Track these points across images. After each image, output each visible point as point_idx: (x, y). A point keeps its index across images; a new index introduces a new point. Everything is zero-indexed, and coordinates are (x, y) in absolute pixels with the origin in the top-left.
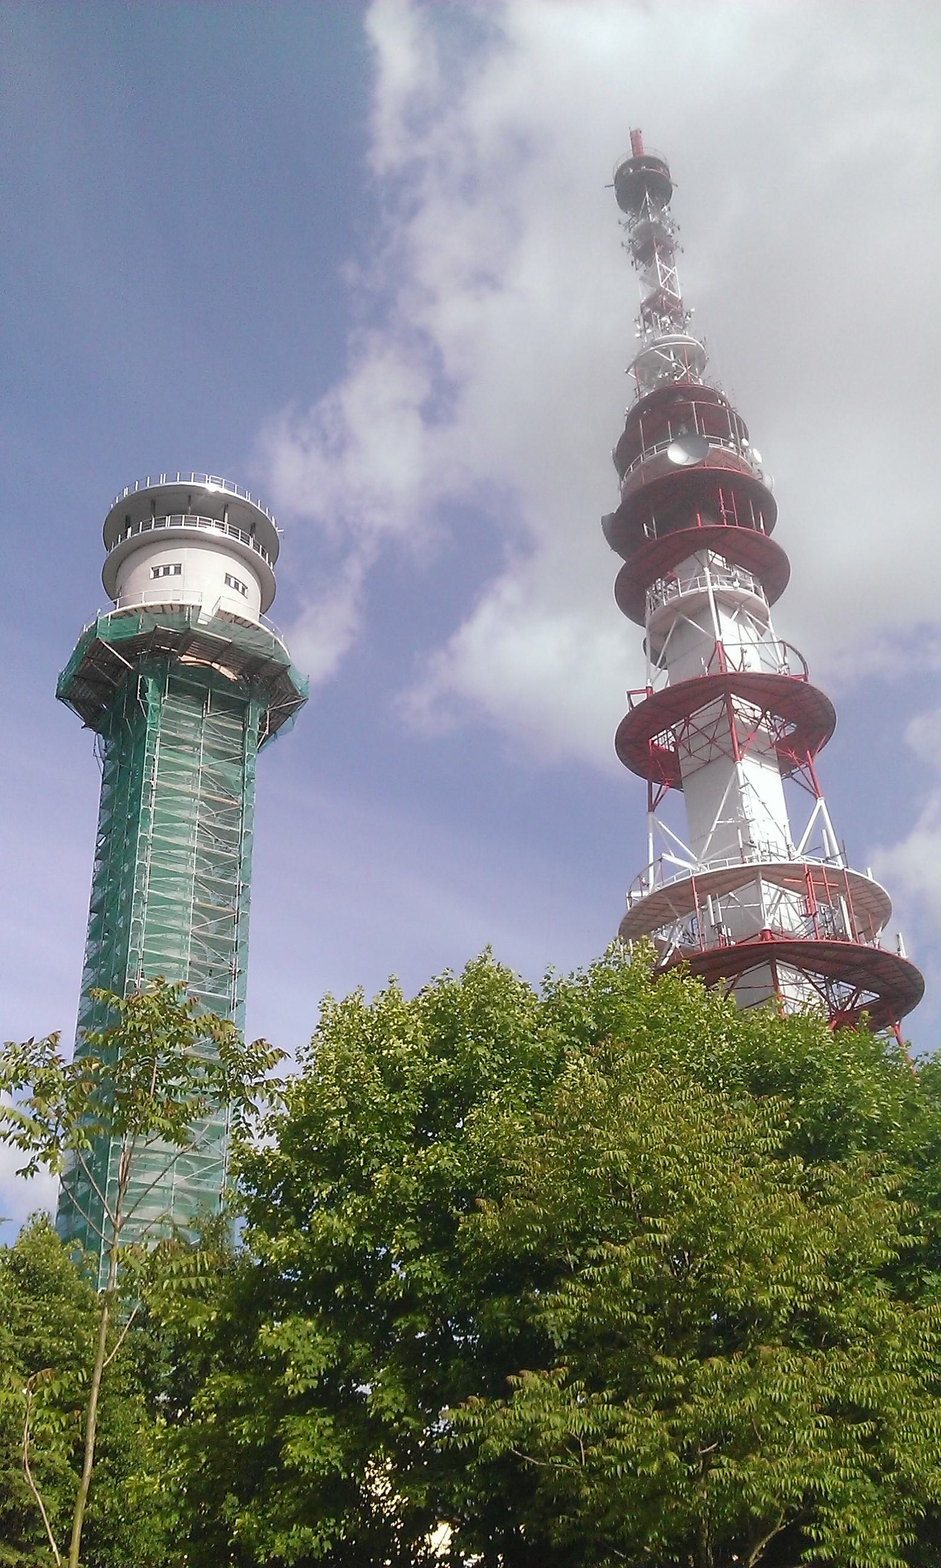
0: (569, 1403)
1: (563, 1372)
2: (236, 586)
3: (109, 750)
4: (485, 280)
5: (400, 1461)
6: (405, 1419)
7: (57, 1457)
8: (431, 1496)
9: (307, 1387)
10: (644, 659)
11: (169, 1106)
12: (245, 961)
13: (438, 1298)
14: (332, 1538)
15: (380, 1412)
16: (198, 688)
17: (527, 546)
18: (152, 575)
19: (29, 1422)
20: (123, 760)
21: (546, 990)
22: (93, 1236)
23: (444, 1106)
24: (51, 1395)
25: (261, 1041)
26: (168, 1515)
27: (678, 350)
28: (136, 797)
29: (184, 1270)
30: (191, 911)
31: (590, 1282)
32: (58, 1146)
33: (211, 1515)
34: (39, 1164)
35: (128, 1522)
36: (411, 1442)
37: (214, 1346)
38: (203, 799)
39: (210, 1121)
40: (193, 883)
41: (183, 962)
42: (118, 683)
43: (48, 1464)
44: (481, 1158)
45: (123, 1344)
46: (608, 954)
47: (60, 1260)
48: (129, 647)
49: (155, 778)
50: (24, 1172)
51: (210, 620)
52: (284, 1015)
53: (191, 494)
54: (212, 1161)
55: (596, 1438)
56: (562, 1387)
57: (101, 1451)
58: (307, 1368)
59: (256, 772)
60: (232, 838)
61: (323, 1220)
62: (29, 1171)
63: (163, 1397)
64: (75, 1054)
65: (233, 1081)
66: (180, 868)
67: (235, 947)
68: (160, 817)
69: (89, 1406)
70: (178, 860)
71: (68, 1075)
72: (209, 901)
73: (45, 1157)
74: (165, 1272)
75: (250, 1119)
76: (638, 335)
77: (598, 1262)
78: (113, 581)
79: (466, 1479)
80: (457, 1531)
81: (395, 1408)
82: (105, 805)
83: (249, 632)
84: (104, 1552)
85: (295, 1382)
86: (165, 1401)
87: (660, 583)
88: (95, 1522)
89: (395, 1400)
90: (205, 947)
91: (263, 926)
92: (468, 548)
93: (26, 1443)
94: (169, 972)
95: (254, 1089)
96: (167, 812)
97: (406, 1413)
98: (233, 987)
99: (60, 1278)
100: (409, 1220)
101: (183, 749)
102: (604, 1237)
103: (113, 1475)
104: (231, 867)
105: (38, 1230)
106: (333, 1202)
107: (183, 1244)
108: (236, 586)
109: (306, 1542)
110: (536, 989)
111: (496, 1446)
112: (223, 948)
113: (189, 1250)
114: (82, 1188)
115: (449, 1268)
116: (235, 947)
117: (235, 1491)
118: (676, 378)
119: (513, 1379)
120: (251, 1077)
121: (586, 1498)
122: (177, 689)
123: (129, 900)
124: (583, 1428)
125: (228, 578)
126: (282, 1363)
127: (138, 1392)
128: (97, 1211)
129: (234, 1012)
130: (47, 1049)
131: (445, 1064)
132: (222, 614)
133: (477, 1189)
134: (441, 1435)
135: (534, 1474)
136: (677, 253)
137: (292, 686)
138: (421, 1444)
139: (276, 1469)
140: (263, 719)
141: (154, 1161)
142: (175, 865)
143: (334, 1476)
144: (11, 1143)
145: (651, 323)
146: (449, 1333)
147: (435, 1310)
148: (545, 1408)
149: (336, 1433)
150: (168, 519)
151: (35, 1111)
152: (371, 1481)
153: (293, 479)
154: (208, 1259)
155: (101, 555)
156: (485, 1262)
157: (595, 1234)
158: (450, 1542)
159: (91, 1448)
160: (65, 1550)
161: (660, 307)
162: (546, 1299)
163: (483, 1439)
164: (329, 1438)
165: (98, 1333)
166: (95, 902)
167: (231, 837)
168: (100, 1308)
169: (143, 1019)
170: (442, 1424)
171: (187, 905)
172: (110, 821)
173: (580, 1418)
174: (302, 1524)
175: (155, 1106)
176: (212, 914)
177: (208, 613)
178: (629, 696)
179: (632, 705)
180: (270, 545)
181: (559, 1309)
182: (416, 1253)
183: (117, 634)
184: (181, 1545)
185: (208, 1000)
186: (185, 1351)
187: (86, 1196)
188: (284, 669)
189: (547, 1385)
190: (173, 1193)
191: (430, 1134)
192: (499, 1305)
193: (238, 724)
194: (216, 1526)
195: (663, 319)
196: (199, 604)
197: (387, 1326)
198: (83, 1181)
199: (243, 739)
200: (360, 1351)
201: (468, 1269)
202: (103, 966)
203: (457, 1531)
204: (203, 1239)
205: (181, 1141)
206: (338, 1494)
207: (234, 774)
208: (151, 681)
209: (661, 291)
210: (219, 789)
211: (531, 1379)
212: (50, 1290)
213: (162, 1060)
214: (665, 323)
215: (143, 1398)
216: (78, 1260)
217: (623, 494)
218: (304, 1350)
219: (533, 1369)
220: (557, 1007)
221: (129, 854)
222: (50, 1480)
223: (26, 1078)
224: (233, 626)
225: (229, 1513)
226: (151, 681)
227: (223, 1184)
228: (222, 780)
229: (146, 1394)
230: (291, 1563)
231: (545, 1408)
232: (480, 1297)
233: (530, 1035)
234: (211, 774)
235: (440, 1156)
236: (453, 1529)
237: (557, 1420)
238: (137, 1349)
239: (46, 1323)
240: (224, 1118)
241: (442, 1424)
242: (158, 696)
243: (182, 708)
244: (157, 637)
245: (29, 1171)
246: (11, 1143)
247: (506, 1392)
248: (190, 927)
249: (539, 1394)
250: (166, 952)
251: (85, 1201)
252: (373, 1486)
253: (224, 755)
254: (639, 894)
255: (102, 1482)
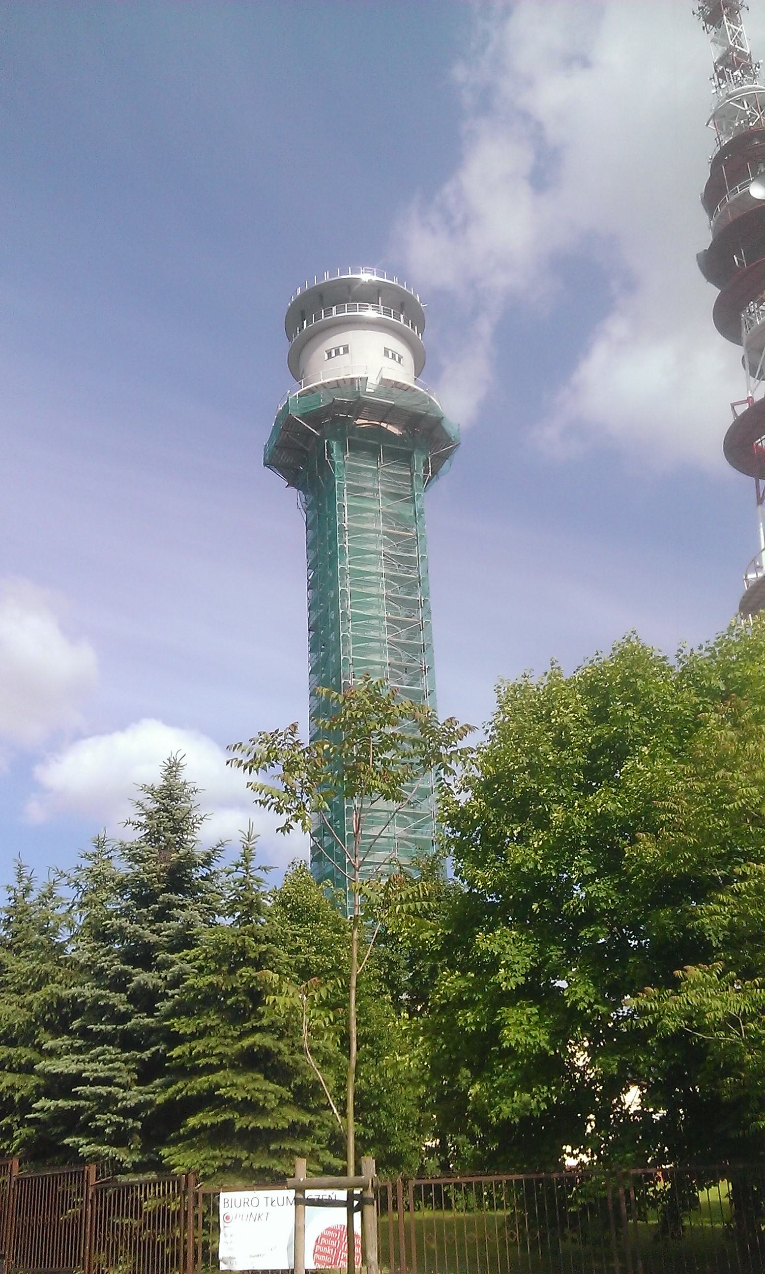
0: (727, 990)
1: (719, 965)
2: (394, 357)
3: (309, 503)
4: (578, 59)
5: (595, 1038)
6: (595, 1006)
7: (330, 1044)
8: (622, 1065)
9: (517, 984)
10: (743, 373)
11: (384, 775)
12: (431, 659)
13: (613, 912)
14: (547, 1100)
15: (575, 1003)
16: (371, 444)
17: (631, 286)
18: (326, 357)
19: (306, 1019)
20: (320, 510)
21: (681, 661)
22: (339, 877)
23: (603, 761)
24: (321, 998)
25: (451, 718)
26: (419, 1087)
27: (751, 99)
28: (333, 538)
29: (411, 897)
30: (385, 623)
31: (737, 894)
32: (305, 808)
33: (450, 1085)
34: (292, 823)
35: (389, 1092)
36: (603, 1023)
37: (439, 955)
38: (385, 533)
39: (420, 784)
40: (385, 601)
41: (384, 664)
42: (312, 447)
43: (324, 1050)
44: (638, 799)
45: (370, 957)
46: (731, 628)
47: (315, 896)
48: (315, 418)
49: (346, 520)
50: (282, 830)
51: (375, 387)
52: (469, 697)
53: (349, 284)
54: (423, 815)
55: (753, 1017)
56: (719, 977)
57: (362, 1039)
58: (516, 967)
59: (425, 507)
60: (411, 563)
61: (517, 854)
62: (286, 828)
63: (404, 996)
64: (311, 741)
65: (433, 751)
66: (373, 590)
67: (423, 649)
68: (354, 552)
69: (350, 1005)
70: (370, 584)
71: (307, 755)
72: (398, 615)
73: (296, 818)
74: (396, 899)
75: (449, 780)
76: (714, 91)
77: (743, 877)
78: (296, 366)
79: (648, 1051)
80: (645, 1091)
81: (587, 999)
82: (311, 545)
83: (406, 394)
84: (373, 1115)
85: (507, 980)
86: (407, 999)
87: (753, 306)
88: (364, 1093)
89: (586, 993)
90: (400, 651)
91: (444, 631)
92: (583, 289)
93: (305, 1035)
94: (375, 673)
95: (450, 757)
96: (359, 547)
97: (596, 1002)
98: (425, 680)
99: (318, 909)
100: (584, 851)
101: (365, 498)
102: (748, 857)
103: (372, 1056)
104: (412, 586)
105: (296, 873)
106: (522, 839)
107: (408, 879)
108: (394, 357)
109: (526, 1105)
110: (672, 661)
111: (671, 1024)
112: (413, 650)
113: (413, 882)
114: (327, 841)
115: (620, 888)
116: (423, 649)
117: (468, 1066)
118: (751, 124)
119: (678, 973)
120: (446, 748)
121: (749, 1061)
122: (355, 447)
123: (337, 619)
124: (740, 1009)
125: (386, 352)
126: (494, 966)
127: (385, 993)
128: (340, 858)
129: (427, 699)
130: (290, 736)
131: (603, 725)
132: (384, 382)
133: (636, 825)
134: (625, 1018)
135: (703, 1048)
136: (743, 11)
137: (446, 434)
138: (610, 1025)
139: (497, 1049)
140: (426, 464)
141: (377, 818)
142: (369, 589)
143: (543, 1052)
144: (269, 808)
145: (724, 79)
146: (625, 938)
147: (611, 921)
148: (708, 995)
149: (542, 1020)
150: (334, 308)
151: (285, 784)
152: (573, 1055)
153: (427, 257)
154: (428, 886)
155: (285, 346)
156: (650, 880)
157: (740, 854)
158: (640, 1100)
159: (354, 1036)
160: (343, 1113)
161: (733, 63)
162: (702, 909)
163: (659, 1020)
164: (536, 1023)
165: (351, 949)
166: (311, 623)
167: (411, 561)
168: (350, 931)
169: (358, 709)
170: (625, 1009)
171: (382, 619)
172: (317, 557)
173: (738, 1001)
174: (521, 1091)
175: (375, 774)
176: (402, 624)
177: (373, 382)
178: (733, 407)
179: (735, 413)
180: (417, 318)
181: (713, 916)
182: (592, 877)
183: (306, 408)
184: (432, 1108)
185: (403, 691)
186: (418, 959)
187: (331, 847)
188: (438, 421)
189: (708, 976)
190: (396, 841)
191: (594, 784)
192: (665, 913)
193: (407, 471)
194: (456, 1093)
195: (735, 74)
196: (365, 376)
197: (575, 933)
198: (327, 835)
199: (412, 481)
200: (555, 953)
201: (636, 886)
202: (323, 672)
203: (645, 1091)
204: (423, 874)
205: (398, 799)
206: (548, 1067)
207: (407, 511)
208: (334, 443)
209: (732, 49)
210: (397, 524)
211: (694, 972)
212: (311, 919)
213: (375, 739)
214: (737, 76)
215: (390, 997)
216: (330, 896)
217: (714, 232)
218: (511, 953)
219: (694, 964)
220: (691, 676)
221: (333, 583)
222: (326, 1062)
223: (276, 758)
224: (394, 390)
225: (464, 1083)
226: (334, 443)
227: (435, 831)
228: (398, 517)
229: (392, 994)
230: (517, 1120)
231: (708, 995)
232: (647, 909)
233: (669, 698)
234: (391, 514)
235: (604, 801)
236: (641, 1090)
237: (719, 1004)
238: (382, 960)
239: (311, 945)
240: (428, 781)
241: (625, 1009)
242: (341, 454)
243: (360, 462)
244: (336, 407)
245: (286, 828)
246: (269, 808)
247: (675, 984)
248: (386, 636)
249: (701, 984)
250: (370, 658)
251: (331, 851)
252: (575, 1059)
253: (397, 496)
254: (754, 576)
255: (365, 1062)
